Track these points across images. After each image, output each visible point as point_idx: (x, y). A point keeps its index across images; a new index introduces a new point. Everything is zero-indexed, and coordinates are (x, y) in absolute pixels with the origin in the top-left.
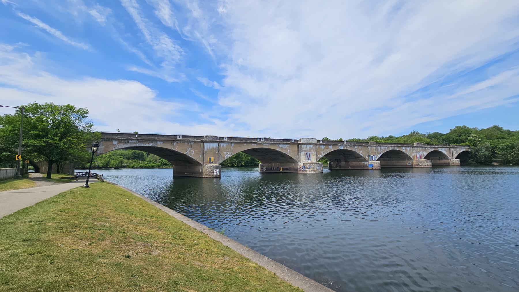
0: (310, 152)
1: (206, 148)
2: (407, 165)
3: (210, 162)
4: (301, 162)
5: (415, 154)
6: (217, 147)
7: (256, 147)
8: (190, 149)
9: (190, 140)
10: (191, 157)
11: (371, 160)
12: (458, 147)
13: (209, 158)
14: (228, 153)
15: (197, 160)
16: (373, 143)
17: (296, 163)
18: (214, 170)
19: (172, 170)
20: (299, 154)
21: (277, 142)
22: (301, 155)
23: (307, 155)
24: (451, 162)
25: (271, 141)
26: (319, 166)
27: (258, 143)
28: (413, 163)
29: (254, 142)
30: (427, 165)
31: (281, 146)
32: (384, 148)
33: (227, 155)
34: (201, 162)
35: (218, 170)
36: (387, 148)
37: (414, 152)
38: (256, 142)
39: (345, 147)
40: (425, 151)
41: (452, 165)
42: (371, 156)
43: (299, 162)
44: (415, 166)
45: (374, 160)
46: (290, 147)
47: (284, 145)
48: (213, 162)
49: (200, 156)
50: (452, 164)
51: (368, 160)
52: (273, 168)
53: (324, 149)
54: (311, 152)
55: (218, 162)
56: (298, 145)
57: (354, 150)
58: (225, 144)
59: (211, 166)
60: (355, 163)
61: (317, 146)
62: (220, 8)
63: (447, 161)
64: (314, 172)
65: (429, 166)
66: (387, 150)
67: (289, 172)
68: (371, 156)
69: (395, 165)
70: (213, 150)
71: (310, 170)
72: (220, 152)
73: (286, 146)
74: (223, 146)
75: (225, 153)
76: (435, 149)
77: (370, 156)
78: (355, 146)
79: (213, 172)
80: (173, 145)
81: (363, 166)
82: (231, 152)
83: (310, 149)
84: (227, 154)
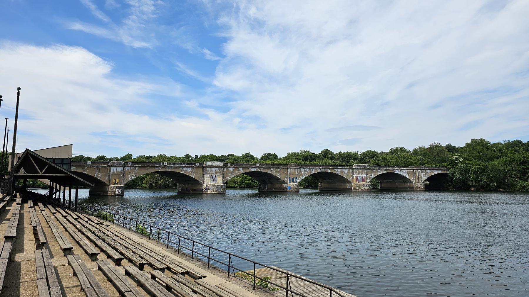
0: (215, 174)
1: (112, 171)
2: (398, 188)
3: (115, 183)
4: (206, 183)
5: (355, 176)
6: (122, 171)
7: (159, 170)
8: (98, 172)
9: (98, 165)
10: (99, 178)
11: (291, 182)
12: (428, 169)
14: (132, 176)
15: (104, 181)
16: (293, 165)
17: (202, 184)
18: (117, 190)
19: (88, 190)
20: (204, 177)
21: (180, 166)
22: (206, 177)
23: (212, 177)
24: (415, 186)
25: (174, 165)
26: (218, 188)
27: (161, 167)
28: (352, 186)
29: (156, 166)
30: (364, 188)
31: (185, 169)
32: (310, 171)
33: (131, 177)
34: (107, 183)
36: (314, 170)
37: (354, 175)
38: (159, 166)
39: (259, 169)
40: (372, 173)
41: (416, 189)
42: (291, 178)
44: (354, 190)
45: (294, 183)
46: (195, 170)
48: (117, 183)
49: (107, 178)
50: (415, 188)
51: (287, 182)
52: (186, 189)
53: (233, 171)
54: (217, 174)
55: (122, 183)
57: (269, 172)
58: (129, 168)
59: (114, 186)
60: (277, 185)
61: (225, 169)
62: (29, 201)
63: (411, 185)
64: (213, 193)
65: (366, 190)
66: (314, 172)
67: (197, 192)
68: (291, 178)
69: (336, 188)
70: (118, 174)
71: (210, 190)
72: (125, 175)
73: (190, 169)
74: (128, 170)
75: (129, 176)
76: (389, 171)
77: (290, 178)
78: (271, 168)
79: (116, 191)
80: (84, 169)
81: (284, 188)
82: (135, 174)
83: (216, 172)
84: (131, 176)
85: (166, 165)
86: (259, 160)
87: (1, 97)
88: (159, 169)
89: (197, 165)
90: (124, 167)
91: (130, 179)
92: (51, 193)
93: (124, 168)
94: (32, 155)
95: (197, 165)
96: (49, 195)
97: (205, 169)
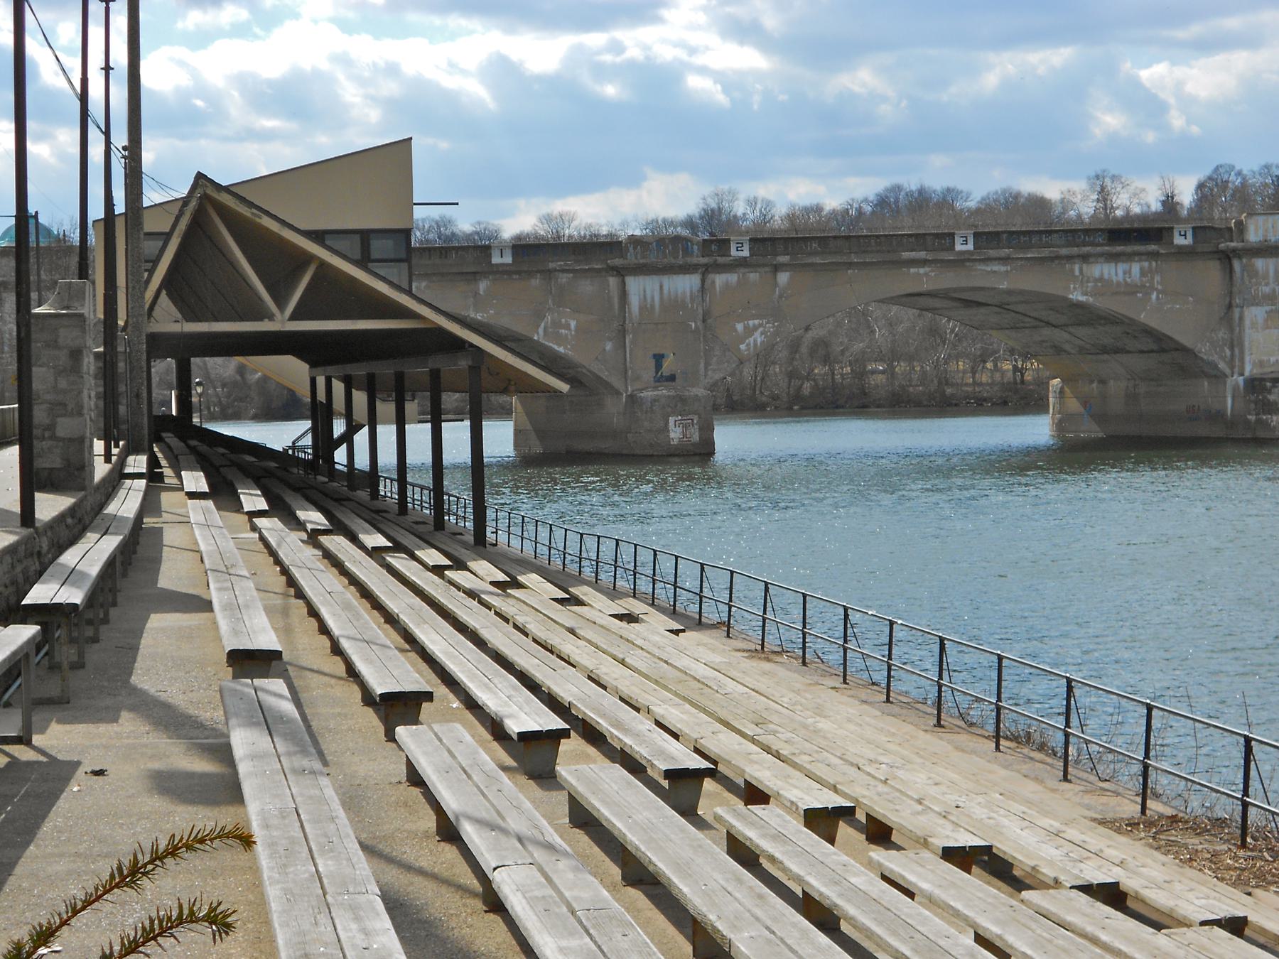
10: (561, 350)
13: (655, 356)
14: (755, 328)
18: (672, 420)
22: (1247, 322)
35: (690, 417)
43: (1232, 368)
47: (1122, 267)
56: (1227, 258)
73: (1136, 268)
75: (740, 327)
79: (666, 429)
80: (476, 294)
84: (749, 332)
85: (970, 247)
86: (738, 346)
87: (5, 956)
88: (926, 274)
89: (1179, 241)
90: (706, 270)
91: (743, 347)
92: (325, 442)
93: (703, 281)
94: (223, 211)
95: (1179, 241)
96: (310, 451)
97: (1237, 265)
